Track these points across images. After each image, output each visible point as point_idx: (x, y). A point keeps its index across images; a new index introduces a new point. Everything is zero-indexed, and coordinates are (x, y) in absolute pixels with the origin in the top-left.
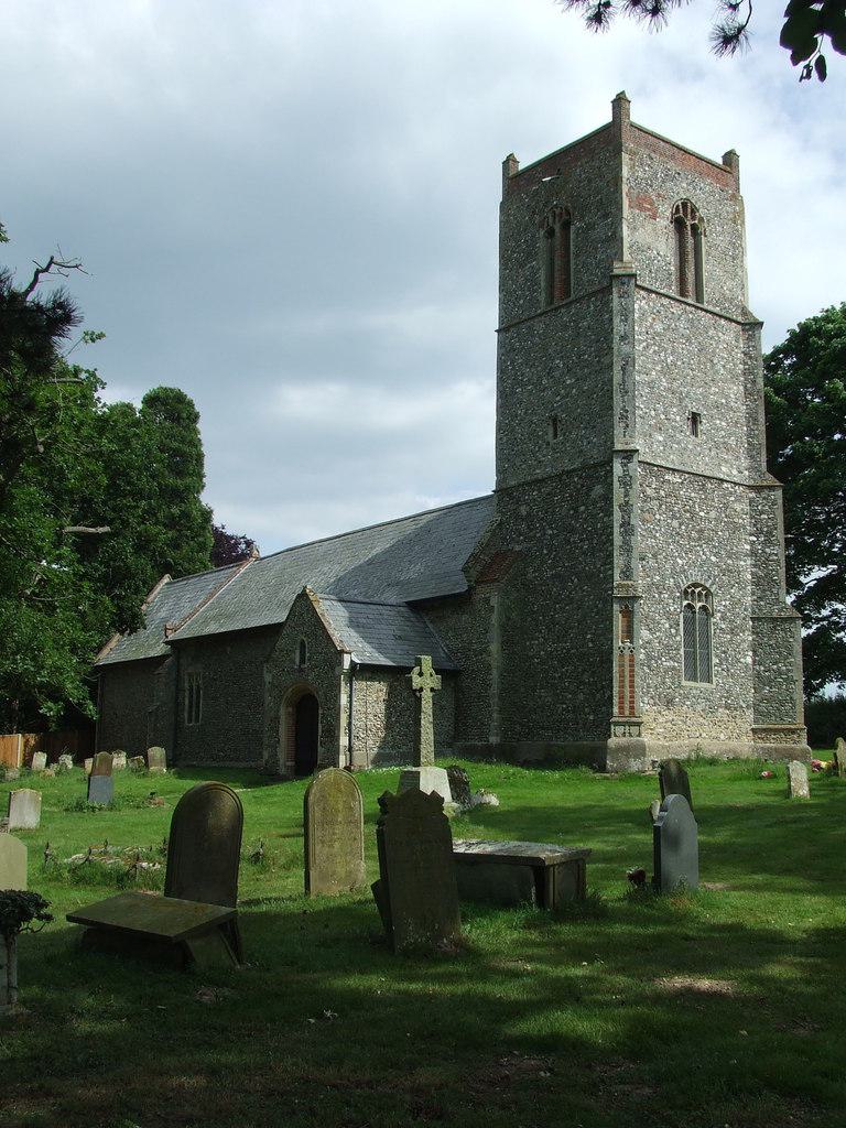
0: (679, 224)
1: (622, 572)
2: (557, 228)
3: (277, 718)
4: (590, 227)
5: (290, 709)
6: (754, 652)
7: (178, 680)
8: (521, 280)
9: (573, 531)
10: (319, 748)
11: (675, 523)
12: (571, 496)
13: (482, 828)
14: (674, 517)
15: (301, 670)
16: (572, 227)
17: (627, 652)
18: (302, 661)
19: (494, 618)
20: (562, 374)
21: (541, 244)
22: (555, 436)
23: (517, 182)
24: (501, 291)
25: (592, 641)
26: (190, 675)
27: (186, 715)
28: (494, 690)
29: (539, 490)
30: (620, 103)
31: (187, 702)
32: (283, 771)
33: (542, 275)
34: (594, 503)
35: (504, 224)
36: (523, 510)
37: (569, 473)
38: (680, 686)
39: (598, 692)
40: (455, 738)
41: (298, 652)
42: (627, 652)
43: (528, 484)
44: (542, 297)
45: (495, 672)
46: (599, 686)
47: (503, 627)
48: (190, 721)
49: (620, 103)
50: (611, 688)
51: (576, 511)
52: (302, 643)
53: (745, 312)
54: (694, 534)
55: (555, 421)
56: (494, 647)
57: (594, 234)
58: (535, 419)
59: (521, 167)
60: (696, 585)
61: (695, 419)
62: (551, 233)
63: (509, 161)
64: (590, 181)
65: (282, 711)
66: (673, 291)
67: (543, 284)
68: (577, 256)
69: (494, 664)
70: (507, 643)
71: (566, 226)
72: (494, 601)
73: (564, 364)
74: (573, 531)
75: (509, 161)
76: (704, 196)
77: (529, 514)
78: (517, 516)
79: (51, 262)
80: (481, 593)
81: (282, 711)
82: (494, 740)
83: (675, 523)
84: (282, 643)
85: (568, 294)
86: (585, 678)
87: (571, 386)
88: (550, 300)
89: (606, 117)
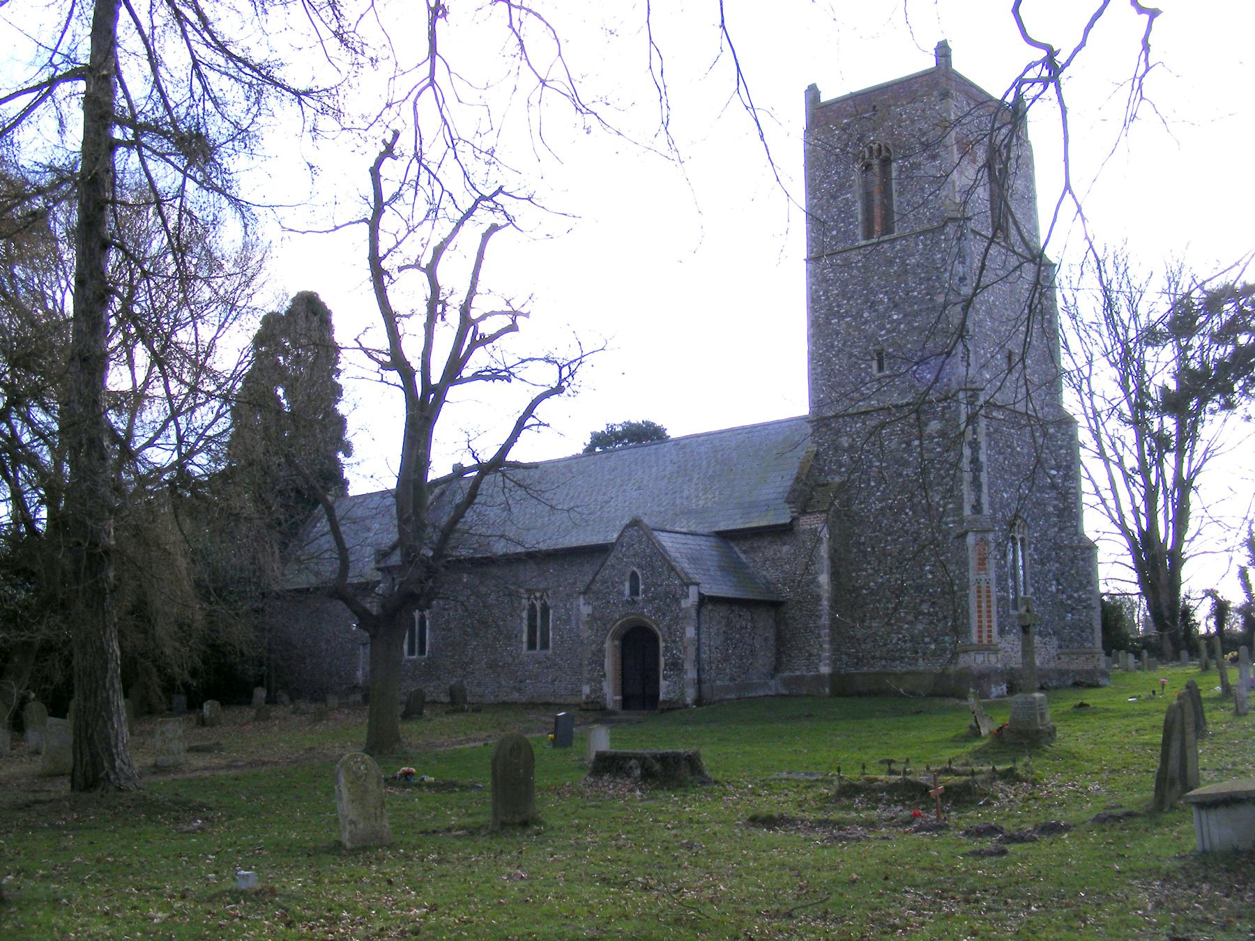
1: (973, 507)
2: (875, 162)
3: (601, 651)
5: (617, 642)
6: (1057, 580)
10: (663, 684)
11: (1001, 459)
14: (1000, 453)
16: (894, 165)
18: (634, 591)
20: (887, 309)
22: (880, 368)
23: (822, 115)
25: (931, 572)
29: (864, 423)
30: (943, 51)
32: (610, 706)
33: (858, 208)
34: (931, 437)
39: (939, 620)
41: (627, 585)
42: (983, 585)
45: (825, 603)
46: (940, 616)
47: (831, 558)
48: (411, 652)
49: (943, 51)
51: (908, 444)
52: (634, 575)
54: (1014, 470)
56: (824, 579)
58: (856, 352)
62: (868, 167)
63: (812, 93)
64: (913, 122)
67: (860, 217)
68: (901, 194)
70: (835, 575)
71: (886, 163)
73: (889, 299)
74: (906, 464)
75: (812, 93)
77: (851, 446)
78: (837, 448)
83: (1001, 459)
85: (888, 229)
86: (925, 608)
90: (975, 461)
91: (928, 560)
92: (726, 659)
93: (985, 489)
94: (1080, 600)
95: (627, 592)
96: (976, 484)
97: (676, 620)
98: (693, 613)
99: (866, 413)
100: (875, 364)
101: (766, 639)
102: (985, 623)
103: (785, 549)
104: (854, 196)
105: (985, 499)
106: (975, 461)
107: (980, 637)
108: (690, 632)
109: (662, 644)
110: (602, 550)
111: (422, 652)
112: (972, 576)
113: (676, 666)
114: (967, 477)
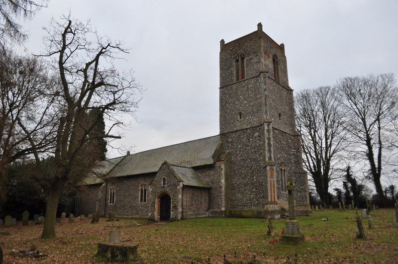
0: (274, 60)
2: (240, 59)
4: (252, 59)
7: (107, 191)
8: (228, 74)
9: (248, 146)
10: (171, 212)
12: (247, 136)
13: (15, 219)
14: (277, 143)
15: (164, 187)
16: (245, 59)
17: (272, 182)
18: (164, 184)
19: (223, 172)
21: (234, 64)
22: (241, 118)
24: (220, 77)
26: (111, 189)
27: (109, 201)
28: (223, 194)
30: (260, 25)
31: (109, 197)
32: (156, 219)
33: (235, 72)
34: (255, 138)
35: (221, 58)
36: (230, 140)
37: (246, 129)
38: (280, 193)
40: (209, 209)
41: (162, 182)
42: (272, 182)
43: (232, 132)
44: (235, 79)
48: (141, 201)
49: (260, 25)
50: (267, 192)
53: (289, 87)
55: (240, 114)
56: (223, 181)
57: (252, 61)
59: (225, 43)
60: (282, 163)
61: (280, 115)
62: (237, 61)
63: (222, 41)
65: (156, 200)
66: (274, 79)
67: (235, 75)
68: (247, 67)
69: (223, 186)
70: (226, 180)
71: (243, 59)
72: (223, 167)
74: (248, 146)
75: (222, 41)
76: (278, 54)
78: (228, 142)
79: (109, 45)
80: (218, 164)
81: (156, 200)
82: (223, 209)
84: (156, 179)
85: (243, 77)
86: (254, 190)
87: (246, 104)
88: (238, 79)
89: (256, 29)
90: (269, 144)
91: (255, 175)
92: (192, 205)
93: (272, 153)
94: (302, 189)
95: (162, 184)
96: (270, 151)
97: (176, 192)
98: (181, 190)
99: (237, 131)
100: (239, 117)
101: (205, 199)
102: (273, 194)
103: (212, 172)
104: (234, 69)
105: (272, 155)
106: (269, 144)
107: (271, 199)
108: (180, 196)
109: (172, 200)
110: (153, 174)
111: (145, 201)
112: (269, 179)
113: (175, 207)
114: (267, 148)
